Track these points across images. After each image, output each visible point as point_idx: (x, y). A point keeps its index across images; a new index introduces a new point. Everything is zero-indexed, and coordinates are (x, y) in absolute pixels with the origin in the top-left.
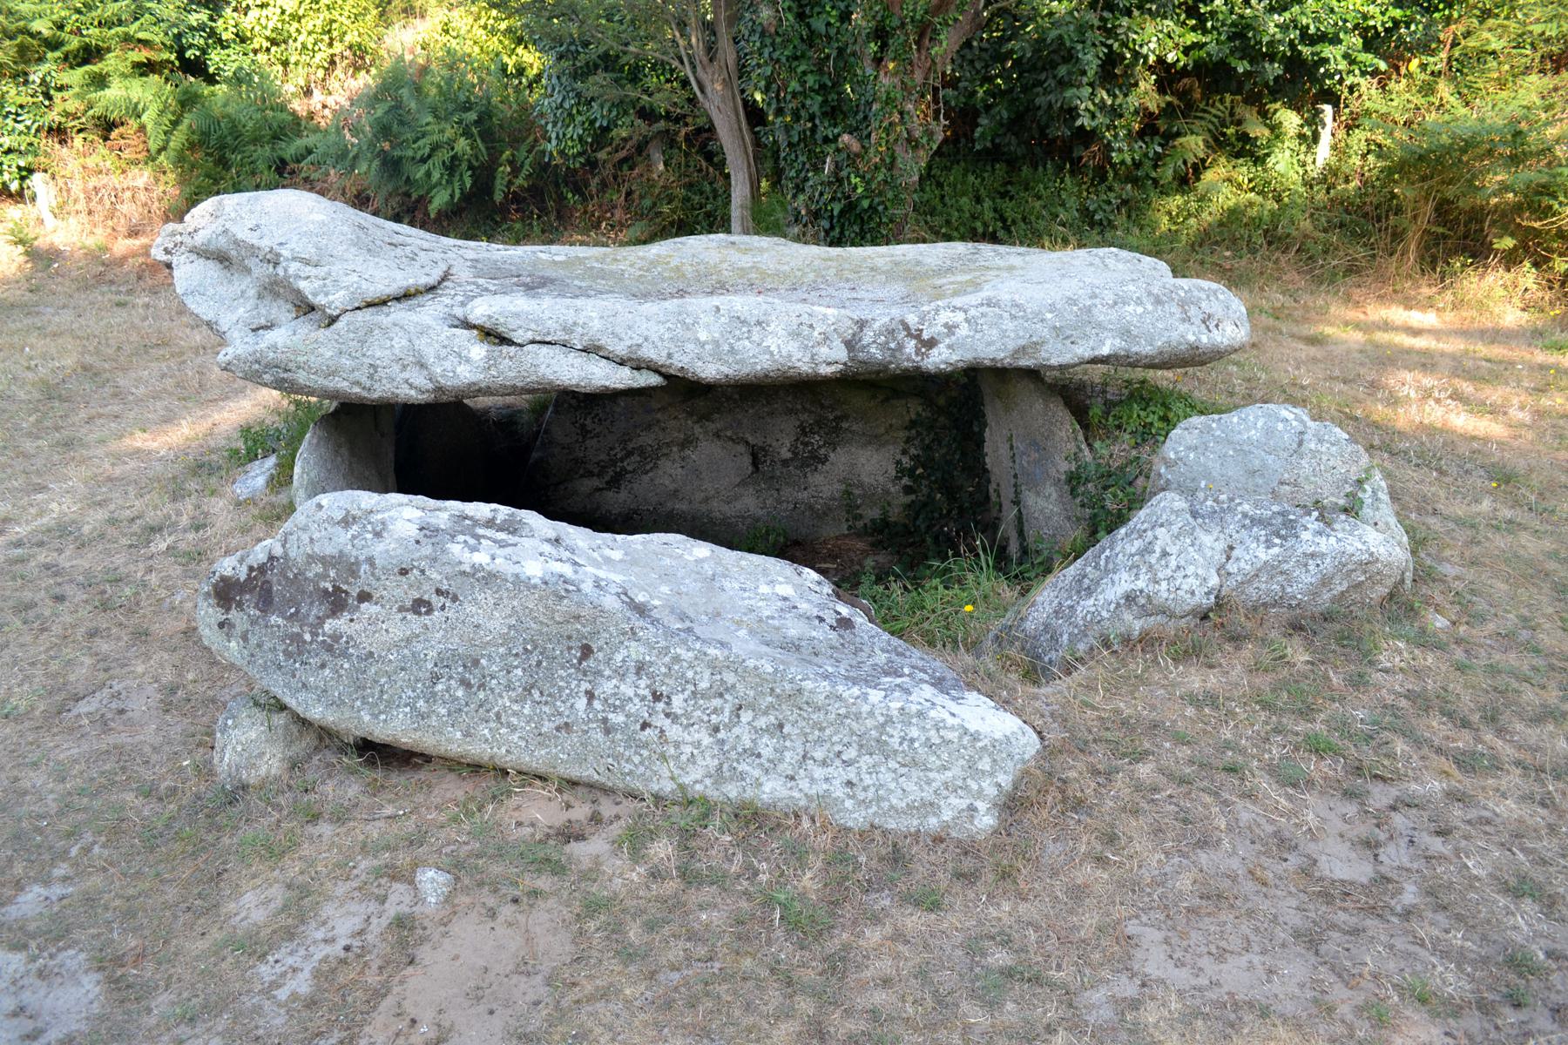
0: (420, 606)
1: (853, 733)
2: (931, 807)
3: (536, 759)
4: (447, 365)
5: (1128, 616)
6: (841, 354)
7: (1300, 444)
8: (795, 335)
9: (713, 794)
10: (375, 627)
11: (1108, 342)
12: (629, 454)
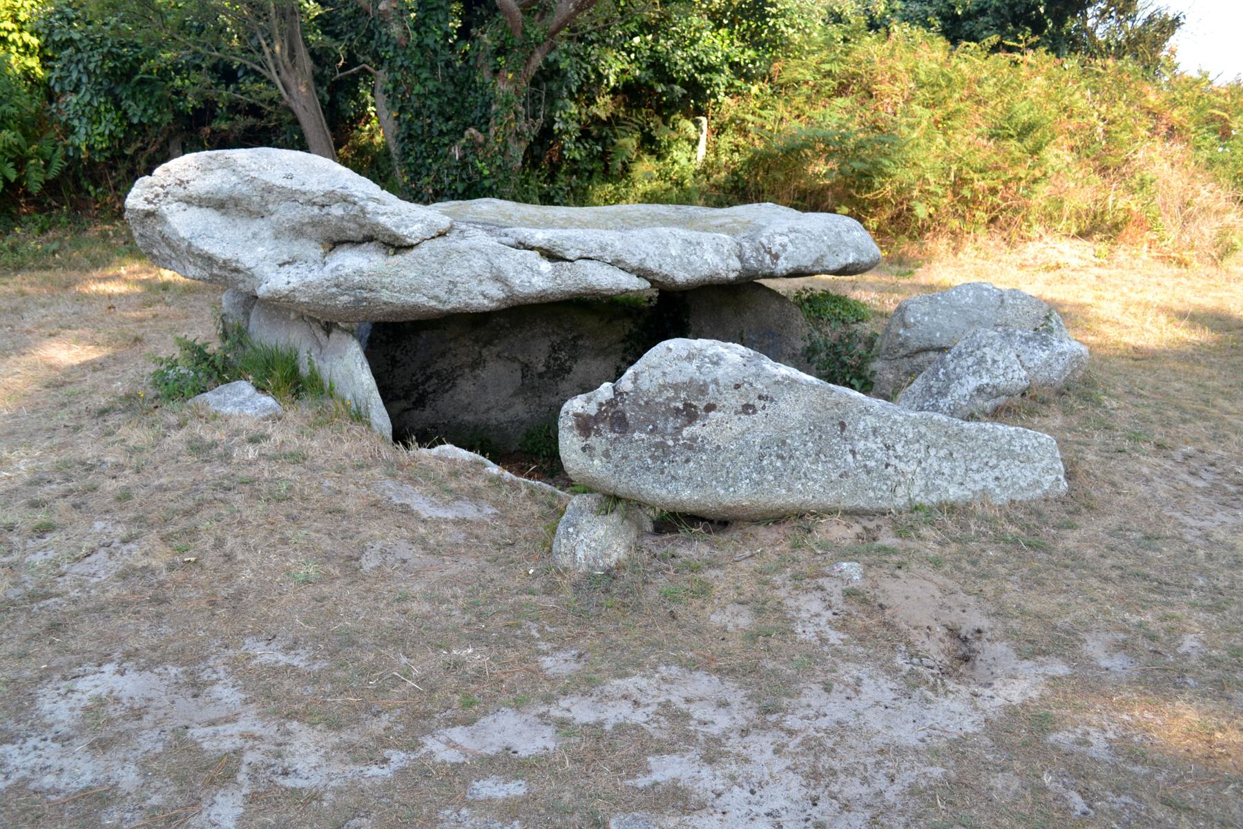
0: (748, 409)
1: (993, 449)
2: (1037, 484)
3: (829, 499)
4: (524, 277)
5: (979, 401)
7: (1002, 301)
9: (925, 501)
10: (718, 428)
12: (429, 378)
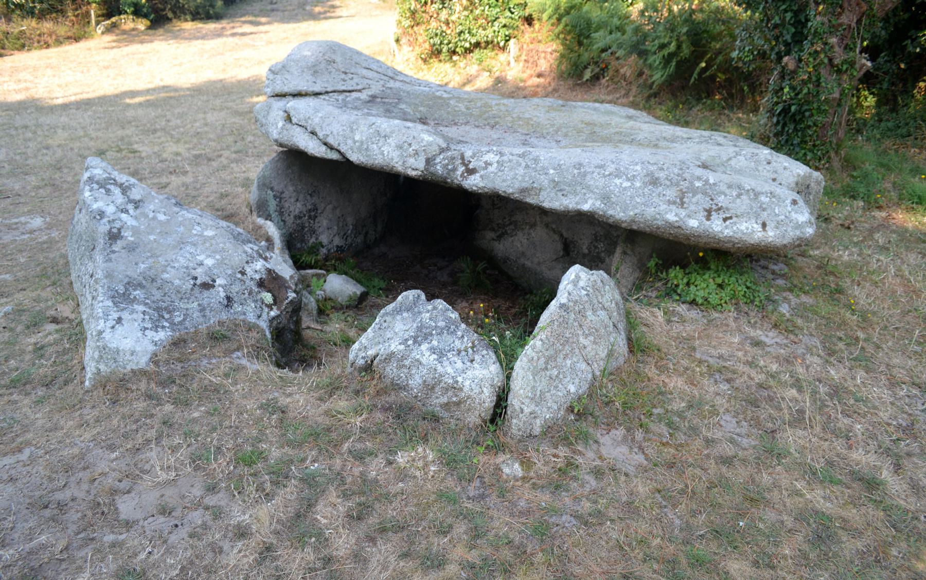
6: (421, 165)
8: (400, 147)
11: (590, 202)
12: (511, 224)
